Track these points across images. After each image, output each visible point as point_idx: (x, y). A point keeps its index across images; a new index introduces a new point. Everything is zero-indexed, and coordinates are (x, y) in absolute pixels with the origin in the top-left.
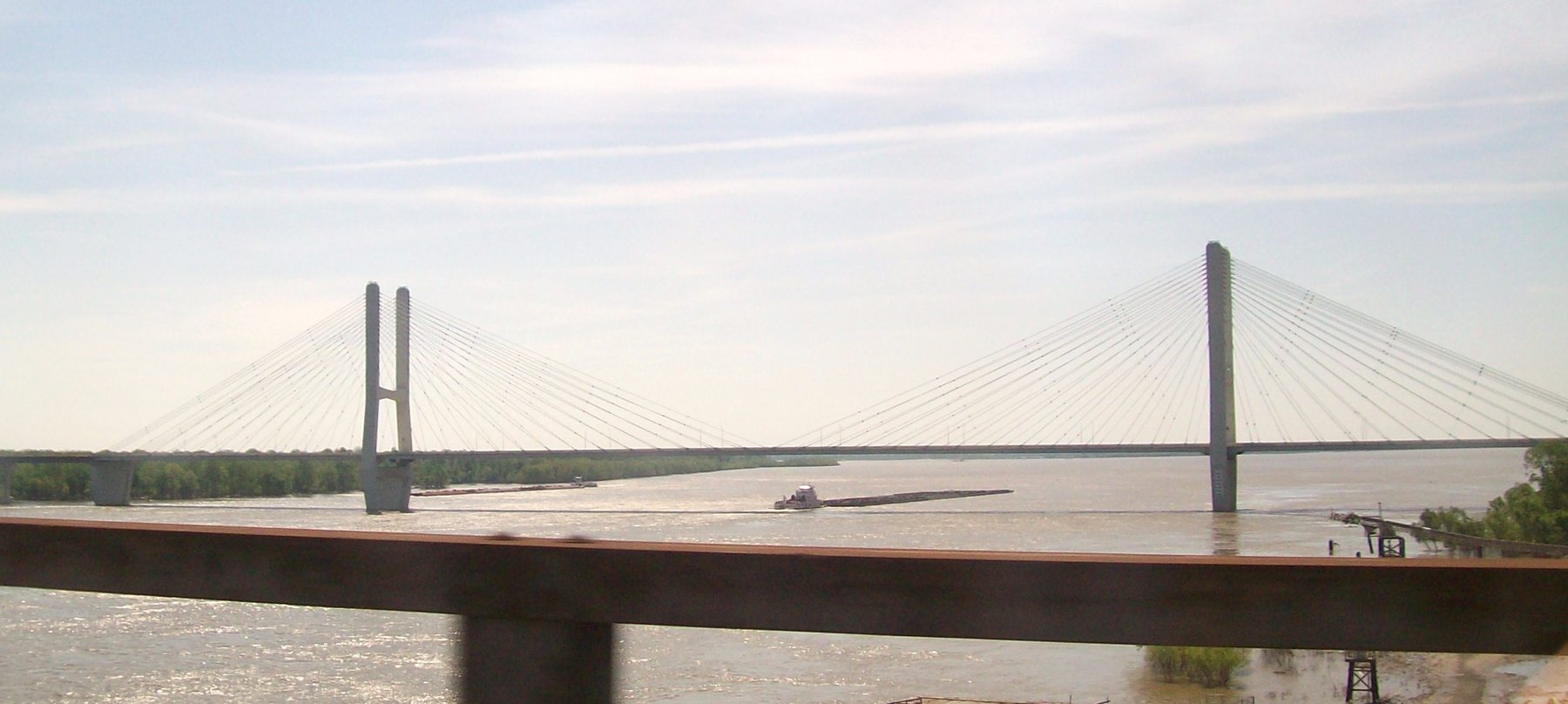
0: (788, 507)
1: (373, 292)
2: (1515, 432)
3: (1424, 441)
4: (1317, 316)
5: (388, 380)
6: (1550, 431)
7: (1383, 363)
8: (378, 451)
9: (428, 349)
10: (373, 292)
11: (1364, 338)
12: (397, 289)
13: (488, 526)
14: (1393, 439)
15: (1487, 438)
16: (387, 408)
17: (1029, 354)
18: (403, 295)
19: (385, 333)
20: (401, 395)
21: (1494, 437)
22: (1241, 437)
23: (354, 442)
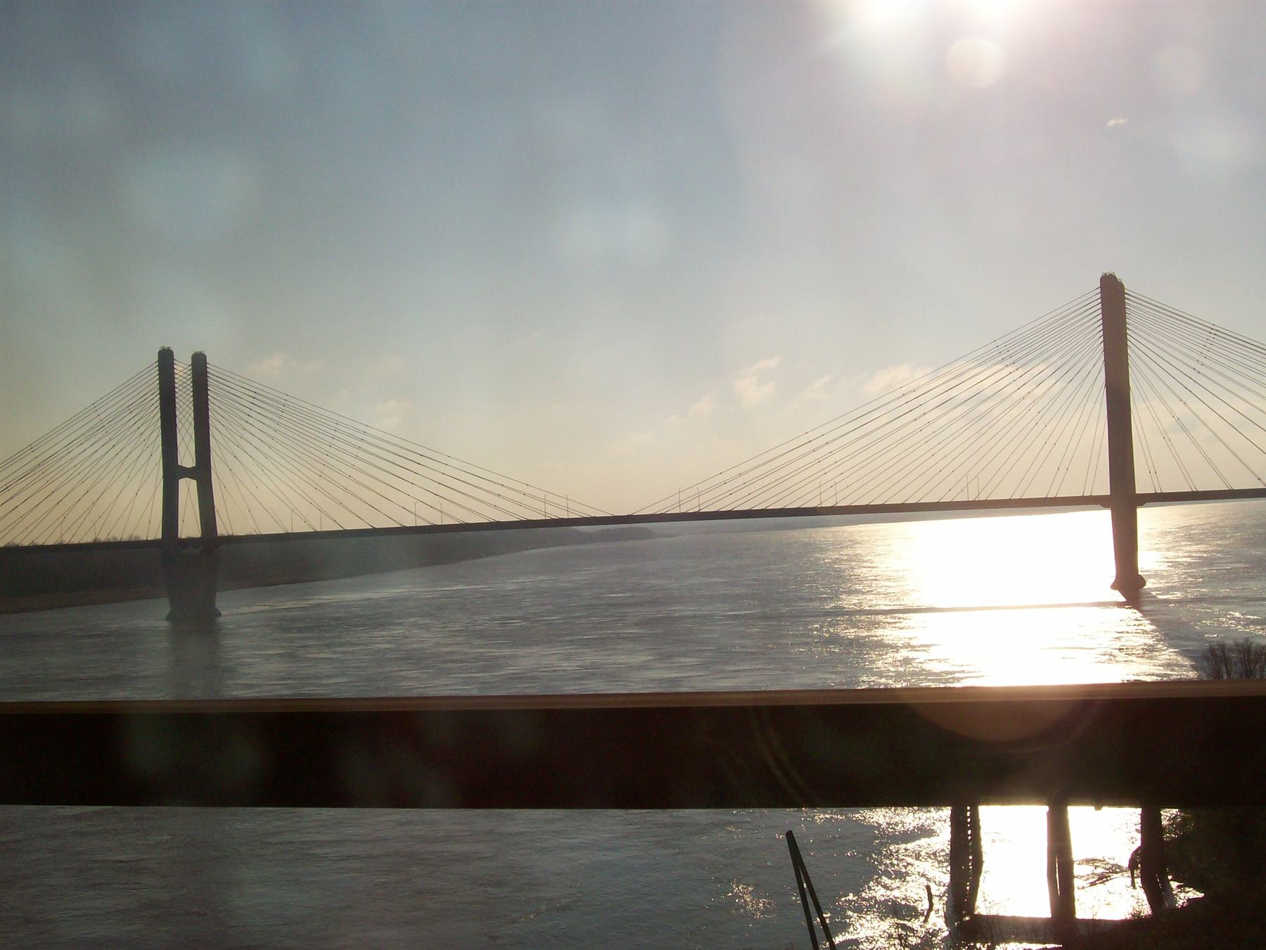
0: (592, 617)
1: (166, 359)
2: (421, 518)
3: (374, 529)
4: (1071, 316)
5: (187, 458)
6: (451, 517)
7: (1199, 373)
8: (1109, 494)
9: (226, 416)
10: (166, 359)
11: (1049, 338)
12: (192, 354)
13: (869, 607)
14: (1237, 486)
15: (399, 526)
16: (188, 489)
17: (254, 398)
18: (199, 364)
19: (181, 403)
20: (202, 472)
21: (346, 528)
22: (1142, 487)
23: (152, 529)
